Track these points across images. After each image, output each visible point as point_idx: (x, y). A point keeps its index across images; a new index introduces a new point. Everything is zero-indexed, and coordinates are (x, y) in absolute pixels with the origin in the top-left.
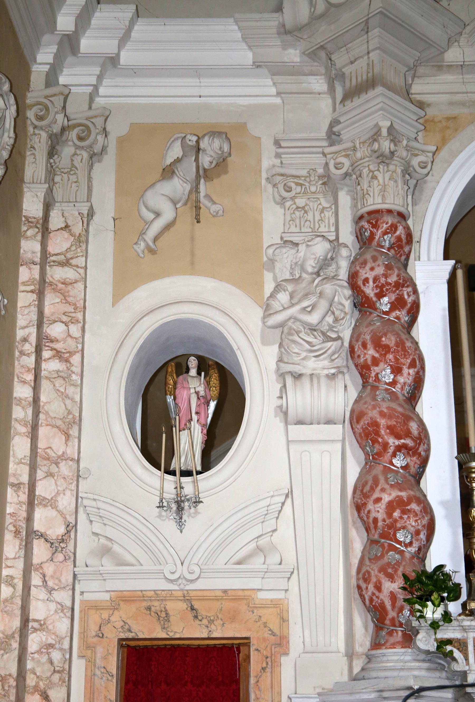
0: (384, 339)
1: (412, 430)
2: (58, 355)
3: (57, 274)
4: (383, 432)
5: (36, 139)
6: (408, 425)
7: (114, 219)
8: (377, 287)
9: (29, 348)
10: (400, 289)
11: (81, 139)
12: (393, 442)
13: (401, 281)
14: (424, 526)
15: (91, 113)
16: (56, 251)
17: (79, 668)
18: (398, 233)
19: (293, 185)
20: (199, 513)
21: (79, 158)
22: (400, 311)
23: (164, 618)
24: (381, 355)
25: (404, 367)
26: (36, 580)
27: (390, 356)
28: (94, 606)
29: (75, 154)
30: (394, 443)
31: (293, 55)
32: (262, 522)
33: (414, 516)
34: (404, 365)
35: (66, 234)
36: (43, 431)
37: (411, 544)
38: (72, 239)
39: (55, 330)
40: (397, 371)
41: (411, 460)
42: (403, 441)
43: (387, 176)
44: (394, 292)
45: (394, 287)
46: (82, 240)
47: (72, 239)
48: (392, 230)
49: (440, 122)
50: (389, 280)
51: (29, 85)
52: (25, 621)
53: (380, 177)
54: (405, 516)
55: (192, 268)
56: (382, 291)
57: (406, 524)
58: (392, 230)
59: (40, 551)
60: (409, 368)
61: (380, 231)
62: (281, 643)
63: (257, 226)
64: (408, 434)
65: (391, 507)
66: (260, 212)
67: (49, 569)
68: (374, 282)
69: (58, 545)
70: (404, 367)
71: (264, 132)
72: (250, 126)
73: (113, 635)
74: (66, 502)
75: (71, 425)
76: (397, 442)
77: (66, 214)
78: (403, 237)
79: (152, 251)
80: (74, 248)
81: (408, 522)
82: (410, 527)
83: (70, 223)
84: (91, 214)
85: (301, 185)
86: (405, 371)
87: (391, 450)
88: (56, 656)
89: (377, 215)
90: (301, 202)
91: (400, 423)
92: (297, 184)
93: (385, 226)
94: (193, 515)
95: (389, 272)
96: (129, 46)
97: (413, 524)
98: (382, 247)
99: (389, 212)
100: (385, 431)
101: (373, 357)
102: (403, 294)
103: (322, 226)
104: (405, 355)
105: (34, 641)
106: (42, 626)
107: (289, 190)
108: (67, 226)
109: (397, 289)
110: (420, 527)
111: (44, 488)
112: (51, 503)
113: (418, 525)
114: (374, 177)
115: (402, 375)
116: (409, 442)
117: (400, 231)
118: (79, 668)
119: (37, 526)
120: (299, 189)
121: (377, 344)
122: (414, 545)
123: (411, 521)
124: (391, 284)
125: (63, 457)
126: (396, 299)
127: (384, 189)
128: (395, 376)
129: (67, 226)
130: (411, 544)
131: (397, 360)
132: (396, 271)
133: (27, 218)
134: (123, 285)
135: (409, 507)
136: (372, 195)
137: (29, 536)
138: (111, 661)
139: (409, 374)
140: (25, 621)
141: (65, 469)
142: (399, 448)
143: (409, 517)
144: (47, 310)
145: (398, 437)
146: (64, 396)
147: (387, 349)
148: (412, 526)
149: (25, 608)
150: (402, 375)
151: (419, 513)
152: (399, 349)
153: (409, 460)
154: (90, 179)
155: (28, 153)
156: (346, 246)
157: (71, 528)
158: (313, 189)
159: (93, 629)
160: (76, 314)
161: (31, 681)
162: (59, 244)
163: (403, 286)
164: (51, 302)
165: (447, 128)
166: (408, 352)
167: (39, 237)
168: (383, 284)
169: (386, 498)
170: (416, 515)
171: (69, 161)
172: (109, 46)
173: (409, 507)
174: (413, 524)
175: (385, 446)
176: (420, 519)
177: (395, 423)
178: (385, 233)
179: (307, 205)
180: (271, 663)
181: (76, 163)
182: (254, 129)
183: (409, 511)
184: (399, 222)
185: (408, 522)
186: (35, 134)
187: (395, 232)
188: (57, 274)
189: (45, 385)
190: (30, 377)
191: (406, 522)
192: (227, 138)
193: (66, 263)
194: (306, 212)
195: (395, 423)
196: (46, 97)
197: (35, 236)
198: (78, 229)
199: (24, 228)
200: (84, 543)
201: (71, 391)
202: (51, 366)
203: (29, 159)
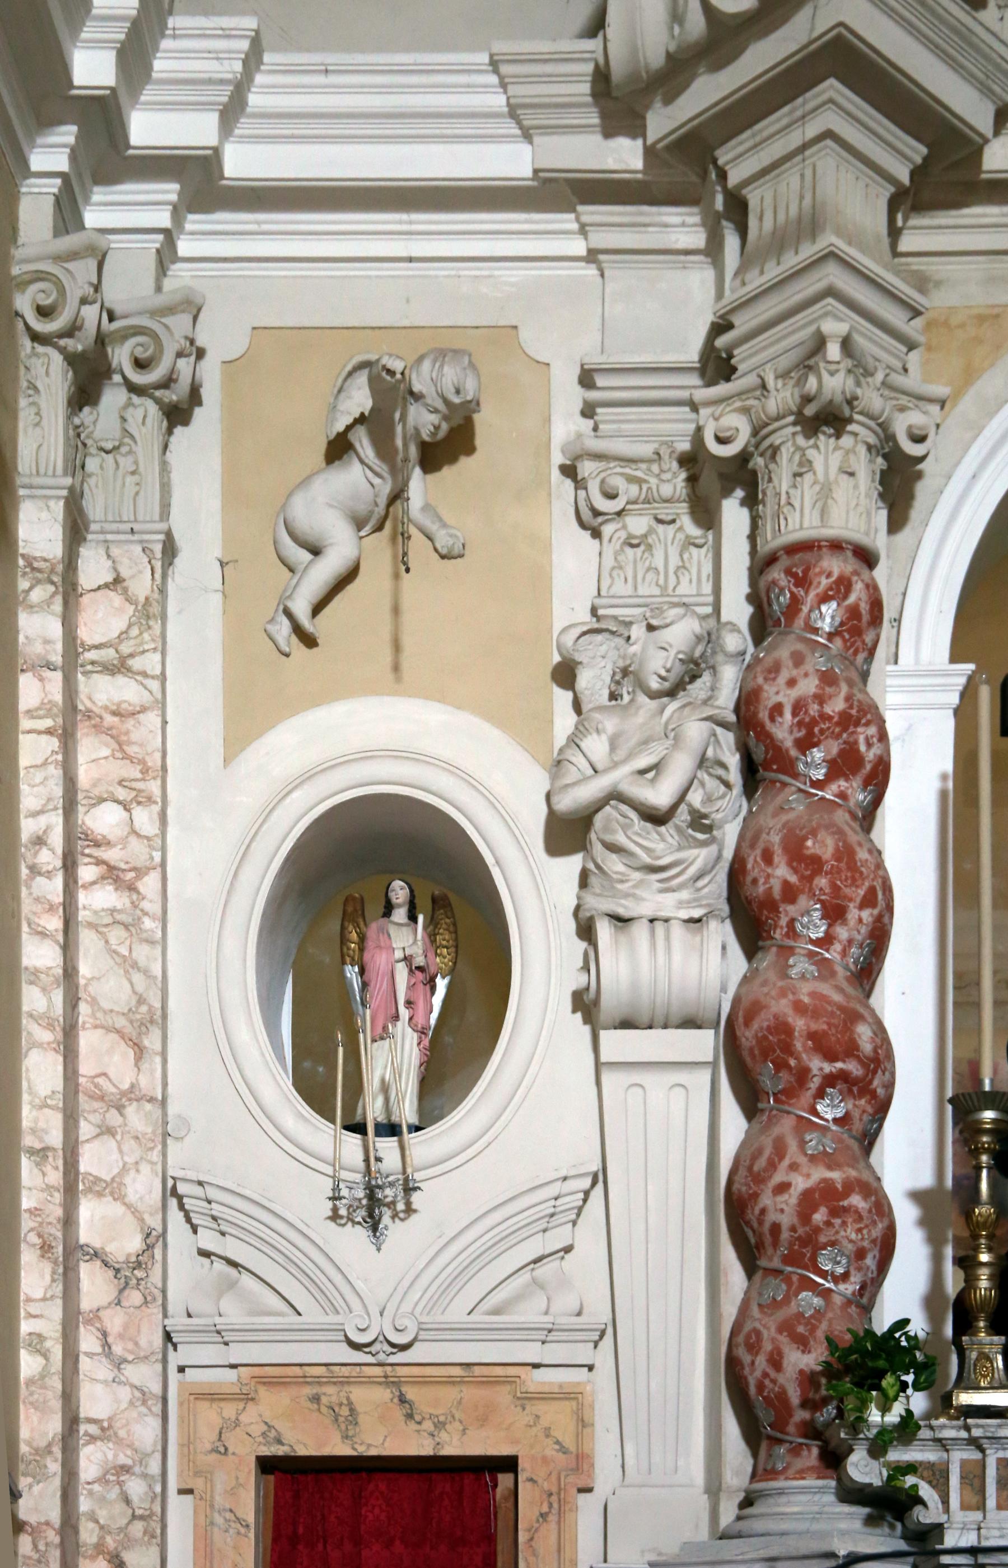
0: (809, 843)
1: (860, 1042)
2: (112, 874)
3: (100, 691)
4: (798, 1045)
5: (38, 366)
6: (852, 1032)
7: (222, 564)
8: (800, 724)
9: (50, 858)
10: (851, 729)
11: (140, 364)
12: (818, 1066)
13: (854, 712)
14: (874, 1241)
15: (160, 301)
16: (98, 639)
17: (180, 1513)
18: (852, 599)
19: (618, 482)
20: (415, 1211)
21: (139, 413)
22: (847, 780)
23: (348, 1418)
24: (802, 878)
25: (851, 905)
26: (88, 1341)
27: (822, 882)
28: (212, 1396)
29: (129, 404)
30: (821, 1069)
31: (625, 156)
32: (545, 1231)
33: (855, 1221)
34: (851, 900)
35: (115, 598)
36: (87, 1040)
37: (845, 1277)
38: (130, 609)
39: (103, 820)
40: (835, 913)
41: (855, 1105)
42: (839, 1065)
43: (835, 460)
44: (838, 736)
45: (838, 724)
46: (152, 612)
47: (130, 609)
48: (838, 591)
49: (962, 326)
50: (828, 710)
51: (15, 230)
52: (72, 1421)
53: (818, 465)
54: (837, 1222)
55: (398, 673)
56: (810, 734)
57: (838, 1237)
58: (838, 591)
59: (94, 1286)
60: (861, 907)
61: (812, 594)
62: (577, 1472)
63: (539, 583)
64: (851, 1050)
65: (808, 1201)
66: (547, 548)
67: (114, 1321)
68: (794, 714)
69: (127, 1274)
70: (851, 905)
71: (561, 347)
72: (525, 335)
73: (247, 1450)
74: (144, 1187)
75: (145, 1027)
76: (828, 1068)
77: (115, 551)
78: (864, 608)
79: (309, 641)
80: (135, 631)
81: (842, 1233)
82: (845, 1242)
83: (125, 573)
84: (170, 550)
85: (639, 481)
86: (853, 913)
87: (815, 1084)
88: (136, 1488)
89: (808, 556)
90: (638, 524)
91: (836, 1027)
92: (631, 479)
93: (824, 582)
94: (402, 1215)
95: (828, 690)
96: (244, 127)
97: (853, 1236)
98: (816, 631)
99: (836, 546)
100: (804, 1046)
101: (786, 884)
102: (856, 742)
103: (684, 580)
104: (854, 880)
105: (91, 1461)
106: (106, 1431)
107: (611, 496)
108: (118, 580)
109: (845, 729)
110: (866, 1244)
111: (95, 1159)
112: (111, 1189)
113: (863, 1239)
114: (807, 464)
115: (845, 922)
116: (852, 1067)
117: (858, 594)
118: (180, 1513)
119: (85, 1235)
120: (634, 490)
121: (796, 854)
122: (852, 1279)
123: (849, 1230)
124: (830, 718)
125: (132, 1094)
126: (842, 753)
127: (826, 492)
128: (830, 926)
129: (118, 580)
130: (845, 1277)
131: (835, 889)
132: (844, 689)
133: (29, 560)
134: (245, 722)
135: (845, 1203)
136: (797, 504)
137: (70, 1256)
138: (245, 1499)
139: (860, 920)
140: (72, 1421)
141: (138, 1119)
142: (831, 1080)
143: (844, 1224)
144: (84, 776)
145: (831, 1057)
146: (129, 965)
147: (815, 864)
148: (851, 1241)
149: (69, 1397)
150: (845, 922)
151: (865, 1214)
152: (843, 865)
153: (850, 1106)
154: (165, 467)
155: (23, 402)
156: (734, 628)
157: (154, 1240)
158: (666, 490)
159: (207, 1437)
160: (146, 785)
161: (88, 1534)
162: (102, 621)
163: (857, 724)
164: (91, 753)
165: (978, 341)
166: (861, 873)
167: (58, 606)
168: (813, 719)
169: (800, 1183)
170: (860, 1218)
171: (117, 424)
172: (191, 130)
173: (845, 1203)
174: (853, 1236)
175: (803, 1075)
176: (867, 1226)
177: (825, 1027)
178: (825, 599)
179: (651, 531)
180: (558, 1508)
181: (132, 428)
182: (535, 341)
183: (846, 1210)
184: (856, 573)
185: (842, 1233)
186: (34, 354)
187: (846, 597)
188: (100, 691)
189: (87, 940)
190: (54, 923)
191: (837, 1232)
192: (472, 365)
193: (119, 667)
194: (649, 547)
195: (825, 1027)
196: (59, 258)
197: (49, 602)
198: (142, 586)
199: (23, 584)
200: (183, 1273)
201: (142, 953)
202: (97, 899)
203: (25, 416)
